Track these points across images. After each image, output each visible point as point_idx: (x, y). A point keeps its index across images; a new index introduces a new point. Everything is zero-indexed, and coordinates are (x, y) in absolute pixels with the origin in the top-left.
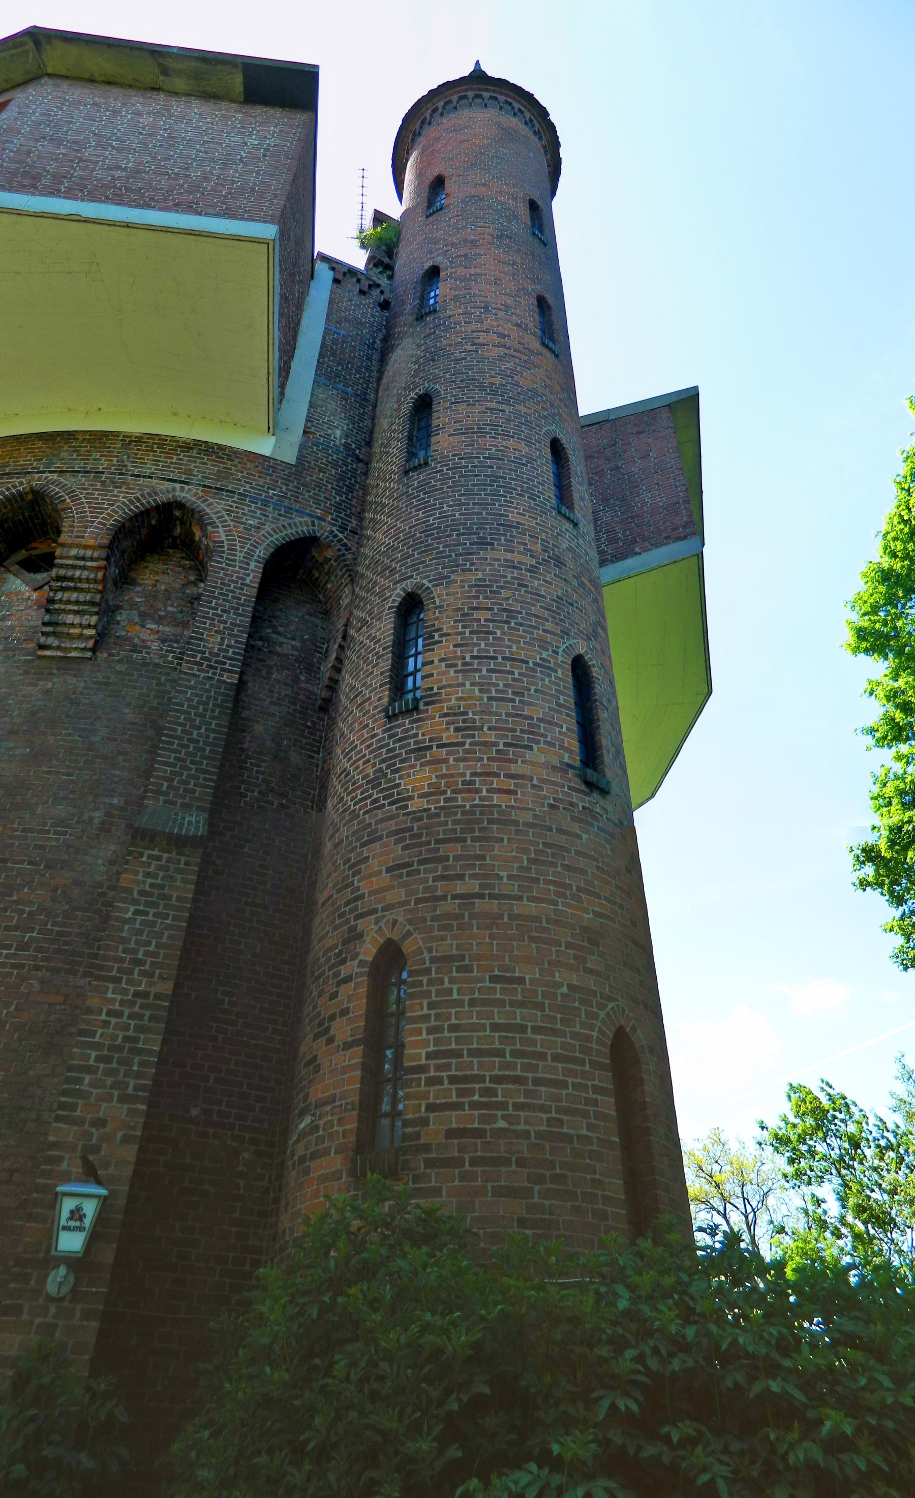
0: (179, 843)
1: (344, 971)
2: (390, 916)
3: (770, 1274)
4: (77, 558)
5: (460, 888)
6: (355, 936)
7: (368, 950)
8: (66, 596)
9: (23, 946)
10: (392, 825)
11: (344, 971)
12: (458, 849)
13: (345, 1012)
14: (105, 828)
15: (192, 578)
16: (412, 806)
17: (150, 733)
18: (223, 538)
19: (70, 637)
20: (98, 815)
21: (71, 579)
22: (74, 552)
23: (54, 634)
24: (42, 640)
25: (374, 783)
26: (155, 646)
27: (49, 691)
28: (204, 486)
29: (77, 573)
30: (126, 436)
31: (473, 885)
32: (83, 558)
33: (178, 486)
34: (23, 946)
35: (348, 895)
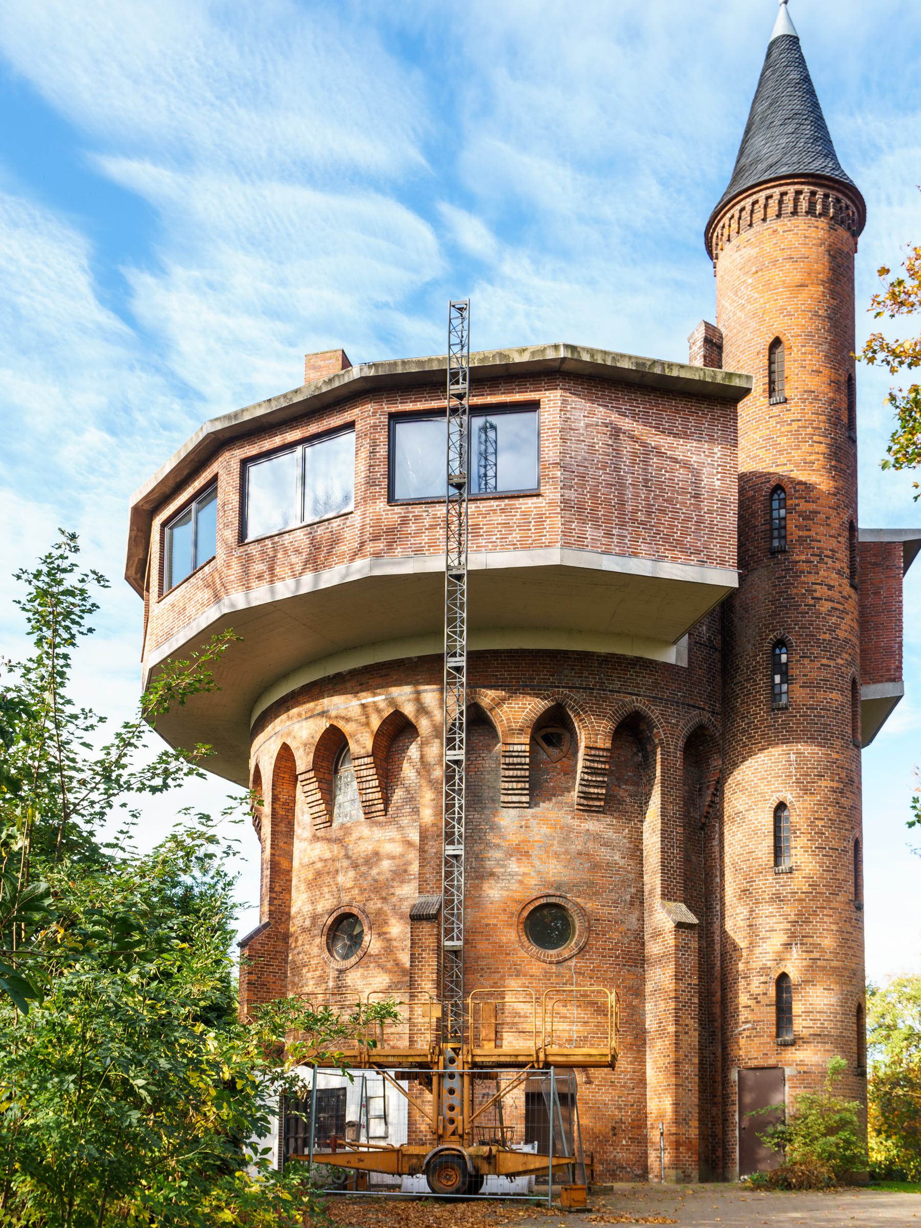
14: (632, 904)
20: (628, 898)
26: (628, 800)
30: (599, 655)
33: (634, 697)
34: (617, 957)
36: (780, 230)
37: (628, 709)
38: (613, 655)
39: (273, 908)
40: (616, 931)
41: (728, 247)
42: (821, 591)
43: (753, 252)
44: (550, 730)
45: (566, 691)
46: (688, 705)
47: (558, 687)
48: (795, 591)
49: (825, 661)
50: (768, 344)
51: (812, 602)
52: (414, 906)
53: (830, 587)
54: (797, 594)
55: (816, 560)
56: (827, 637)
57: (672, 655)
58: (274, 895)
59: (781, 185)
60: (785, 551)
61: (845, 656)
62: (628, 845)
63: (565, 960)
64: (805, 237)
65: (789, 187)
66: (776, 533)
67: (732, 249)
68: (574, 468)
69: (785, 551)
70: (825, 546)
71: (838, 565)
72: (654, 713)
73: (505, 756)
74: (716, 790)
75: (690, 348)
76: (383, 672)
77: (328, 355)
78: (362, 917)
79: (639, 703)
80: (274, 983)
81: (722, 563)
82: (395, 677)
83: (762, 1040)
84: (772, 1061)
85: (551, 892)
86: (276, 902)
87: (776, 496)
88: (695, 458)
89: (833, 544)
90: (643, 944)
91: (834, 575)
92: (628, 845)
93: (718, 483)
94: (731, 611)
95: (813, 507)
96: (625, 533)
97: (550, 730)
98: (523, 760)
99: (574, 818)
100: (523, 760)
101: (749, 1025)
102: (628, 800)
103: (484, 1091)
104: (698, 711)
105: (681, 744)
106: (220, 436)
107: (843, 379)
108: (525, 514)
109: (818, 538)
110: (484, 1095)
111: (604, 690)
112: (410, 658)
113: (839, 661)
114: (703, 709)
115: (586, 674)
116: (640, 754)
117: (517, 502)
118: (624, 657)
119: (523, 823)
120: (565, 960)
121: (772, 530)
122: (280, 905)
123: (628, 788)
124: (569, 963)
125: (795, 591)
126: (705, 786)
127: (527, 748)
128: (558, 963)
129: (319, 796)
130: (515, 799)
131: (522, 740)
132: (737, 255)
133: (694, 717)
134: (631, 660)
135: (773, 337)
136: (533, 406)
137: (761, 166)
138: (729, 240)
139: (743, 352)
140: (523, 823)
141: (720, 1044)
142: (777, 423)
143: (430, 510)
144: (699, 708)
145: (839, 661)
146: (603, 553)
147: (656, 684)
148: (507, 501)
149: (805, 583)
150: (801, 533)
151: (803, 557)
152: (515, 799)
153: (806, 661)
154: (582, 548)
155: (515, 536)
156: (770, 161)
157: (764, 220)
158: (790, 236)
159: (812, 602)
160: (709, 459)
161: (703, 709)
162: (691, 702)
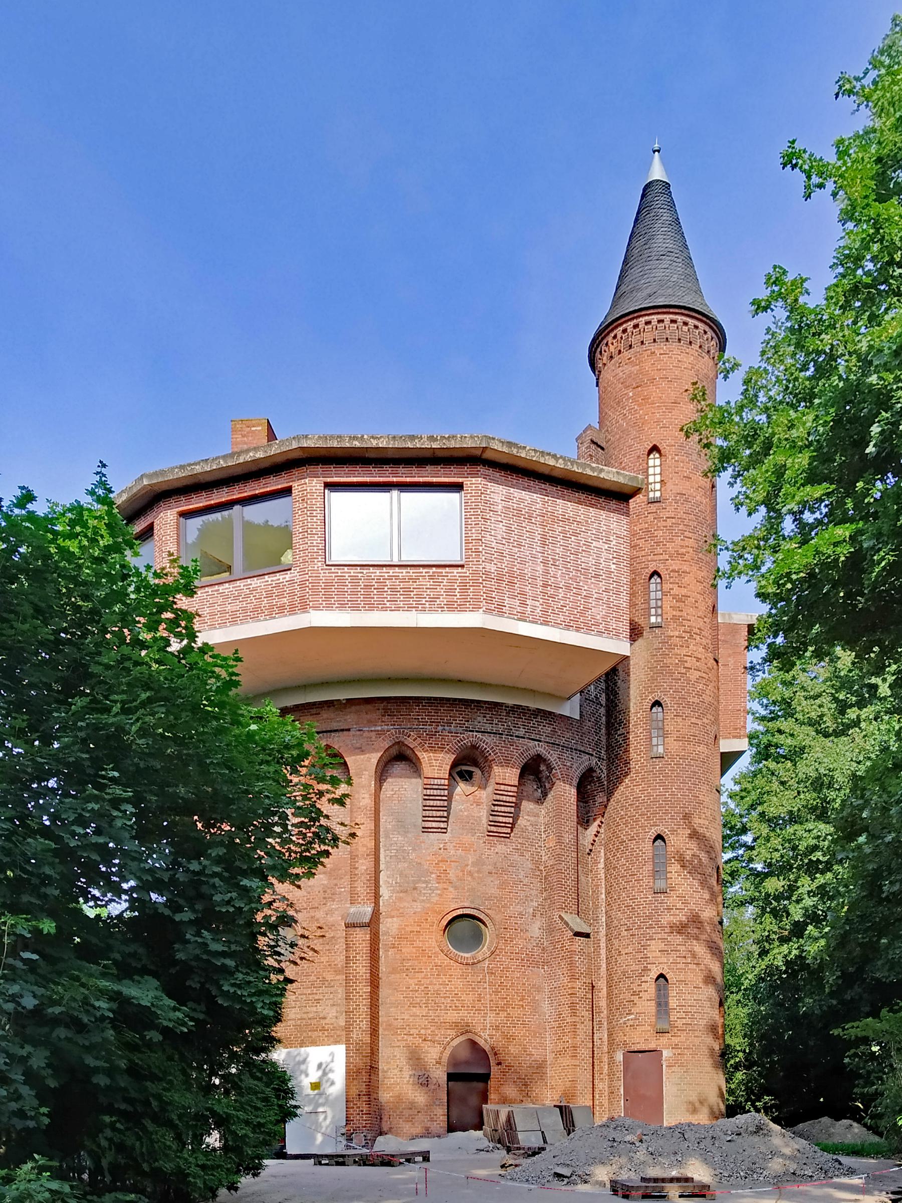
26: (530, 828)
33: (536, 743)
37: (532, 752)
38: (519, 707)
40: (521, 938)
41: (611, 365)
42: (690, 662)
44: (465, 768)
45: (479, 735)
46: (580, 751)
48: (669, 661)
49: (694, 720)
51: (684, 671)
53: (698, 659)
55: (687, 636)
56: (696, 700)
57: (571, 709)
59: (658, 313)
61: (710, 717)
62: (530, 866)
63: (479, 962)
64: (679, 361)
65: (665, 316)
66: (653, 611)
67: (614, 365)
68: (493, 545)
70: (694, 625)
71: (704, 641)
72: (552, 756)
73: (494, 805)
75: (578, 448)
76: (314, 711)
79: (541, 749)
81: (617, 635)
82: (325, 716)
83: (643, 1028)
84: (652, 1046)
85: (466, 905)
87: (653, 580)
88: (595, 544)
89: (701, 624)
91: (701, 649)
92: (530, 866)
93: (613, 566)
94: (615, 675)
95: (684, 591)
96: (537, 604)
97: (465, 768)
98: (442, 793)
100: (442, 793)
101: (633, 1016)
104: (588, 756)
106: (156, 488)
108: (452, 581)
109: (689, 618)
113: (705, 720)
114: (592, 755)
116: (539, 791)
117: (444, 571)
119: (441, 846)
120: (479, 962)
121: (650, 608)
123: (529, 818)
124: (482, 964)
125: (669, 661)
126: (591, 818)
127: (446, 782)
128: (473, 964)
130: (434, 825)
131: (442, 776)
133: (585, 762)
135: (651, 445)
136: (457, 487)
137: (640, 295)
139: (624, 455)
140: (441, 846)
141: (606, 1031)
143: (365, 571)
145: (705, 720)
146: (519, 619)
147: (554, 731)
148: (434, 569)
150: (674, 613)
151: (677, 633)
152: (434, 825)
153: (679, 720)
154: (501, 614)
155: (443, 600)
156: (648, 291)
158: (665, 358)
159: (684, 671)
160: (607, 546)
161: (592, 755)
162: (582, 749)
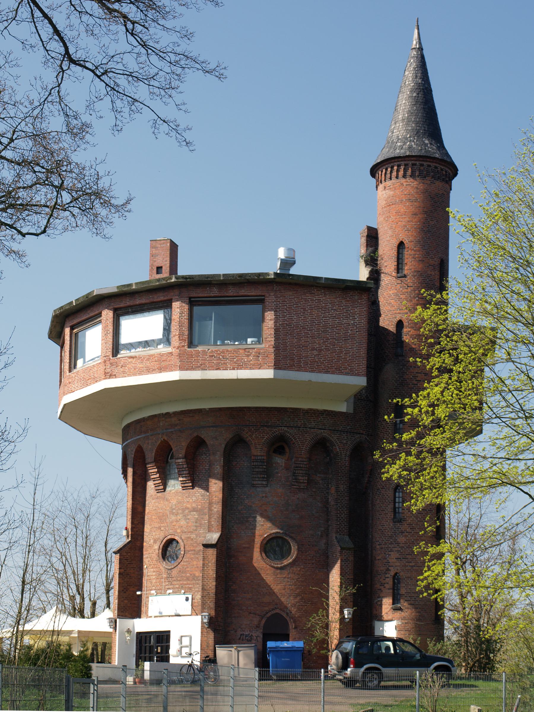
0: (349, 549)
1: (387, 576)
2: (397, 568)
3: (389, 417)
4: (301, 461)
5: (411, 564)
6: (388, 570)
7: (392, 573)
8: (299, 471)
9: (313, 564)
10: (396, 549)
11: (387, 576)
12: (410, 557)
13: (388, 583)
14: (322, 536)
15: (325, 456)
16: (400, 545)
17: (326, 509)
18: (338, 450)
19: (301, 483)
20: (319, 533)
21: (300, 467)
22: (300, 459)
23: (296, 482)
24: (293, 483)
25: (391, 537)
26: (321, 482)
27: (298, 498)
28: (330, 430)
29: (301, 465)
30: (303, 410)
31: (413, 564)
32: (303, 461)
33: (322, 431)
34: (313, 564)
35: (386, 561)
36: (405, 184)
38: (311, 409)
39: (134, 526)
43: (392, 193)
45: (286, 429)
47: (282, 427)
50: (396, 246)
51: (416, 382)
52: (311, 381)
54: (408, 378)
58: (134, 526)
60: (403, 356)
69: (403, 356)
74: (371, 474)
76: (191, 415)
77: (162, 242)
78: (180, 541)
80: (134, 573)
86: (135, 529)
90: (328, 557)
99: (291, 492)
102: (321, 482)
103: (241, 633)
104: (359, 436)
105: (348, 453)
107: (437, 261)
110: (241, 635)
111: (306, 428)
112: (205, 409)
115: (296, 419)
118: (318, 410)
122: (137, 531)
129: (158, 475)
130: (259, 482)
132: (384, 192)
134: (321, 411)
138: (381, 182)
142: (401, 287)
144: (359, 434)
149: (412, 372)
152: (259, 482)
157: (391, 179)
159: (416, 382)
